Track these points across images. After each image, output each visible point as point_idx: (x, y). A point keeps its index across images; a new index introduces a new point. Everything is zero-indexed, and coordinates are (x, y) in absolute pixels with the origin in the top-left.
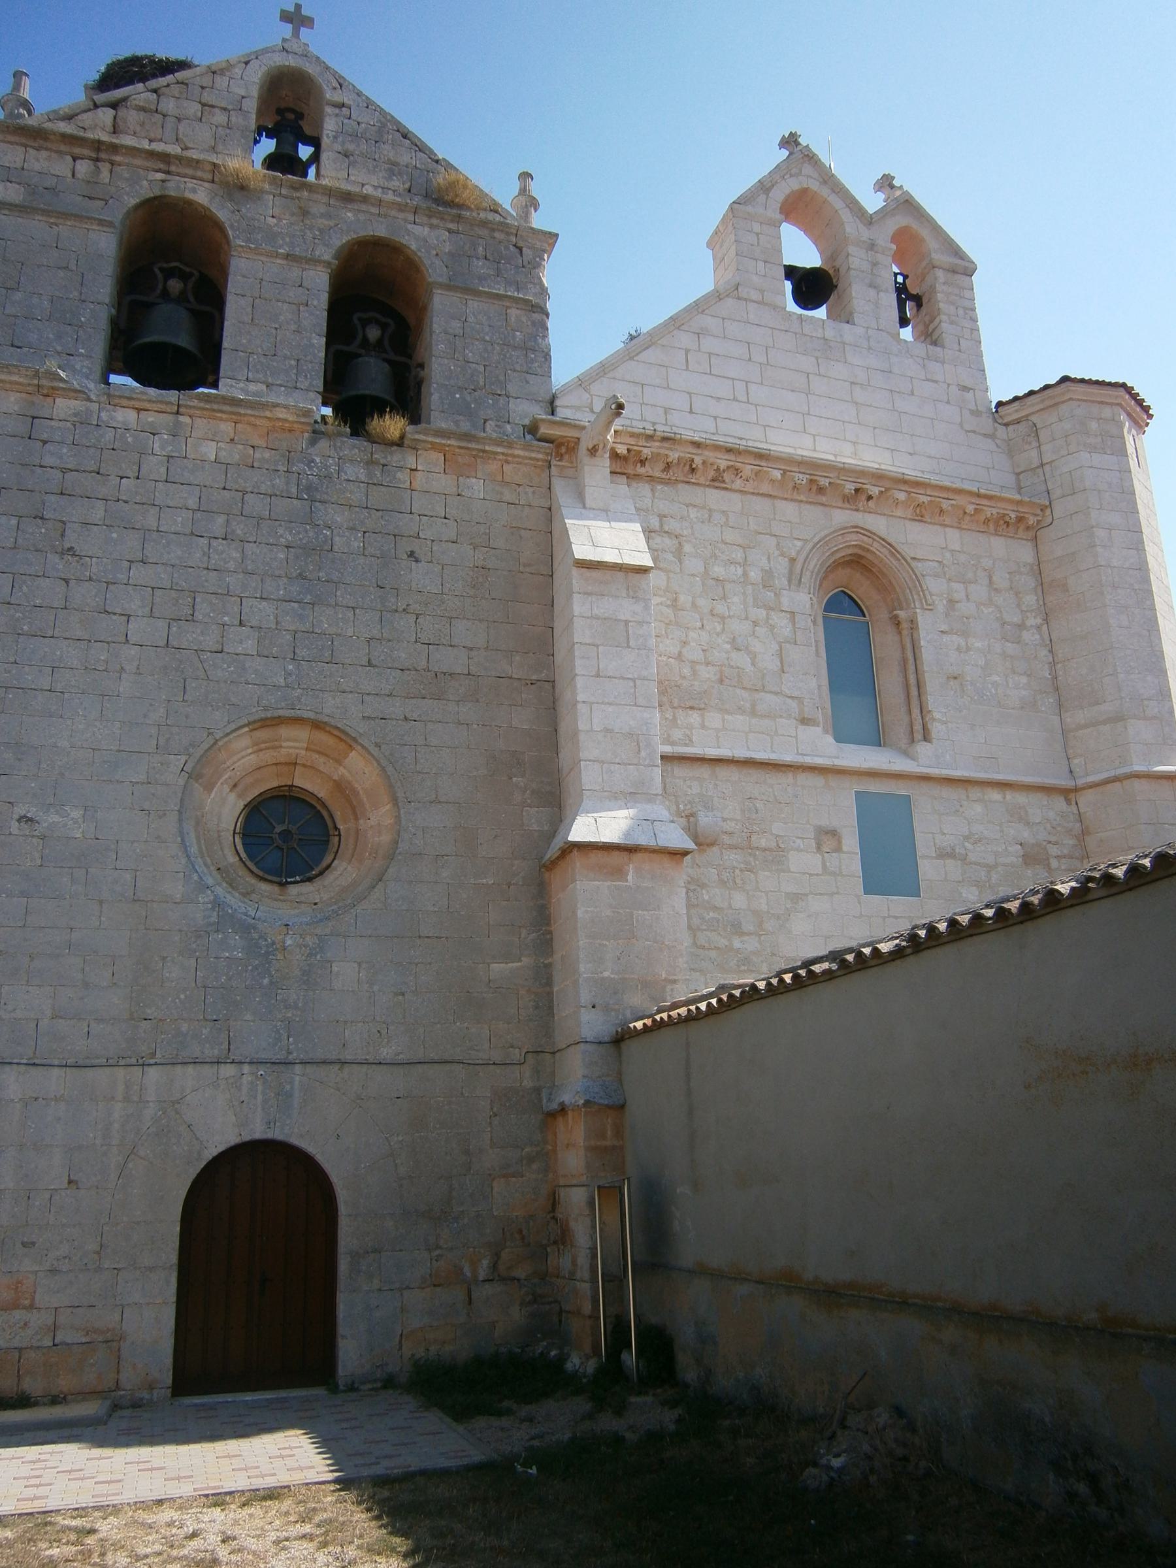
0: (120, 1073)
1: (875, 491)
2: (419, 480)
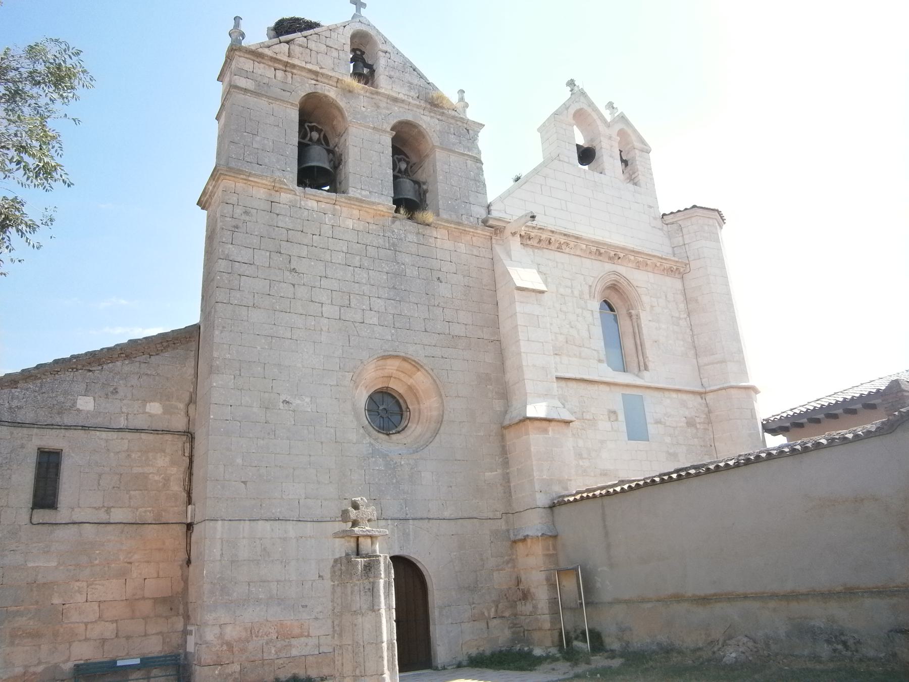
1: (621, 255)
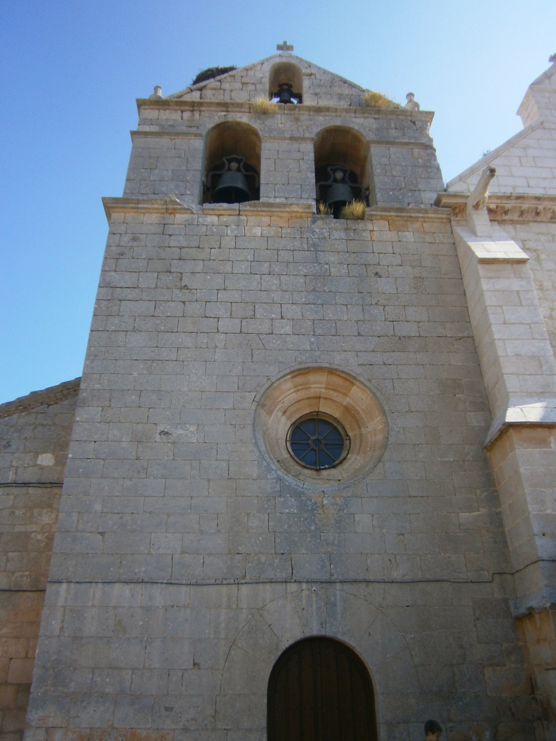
0: (224, 589)
2: (376, 235)
